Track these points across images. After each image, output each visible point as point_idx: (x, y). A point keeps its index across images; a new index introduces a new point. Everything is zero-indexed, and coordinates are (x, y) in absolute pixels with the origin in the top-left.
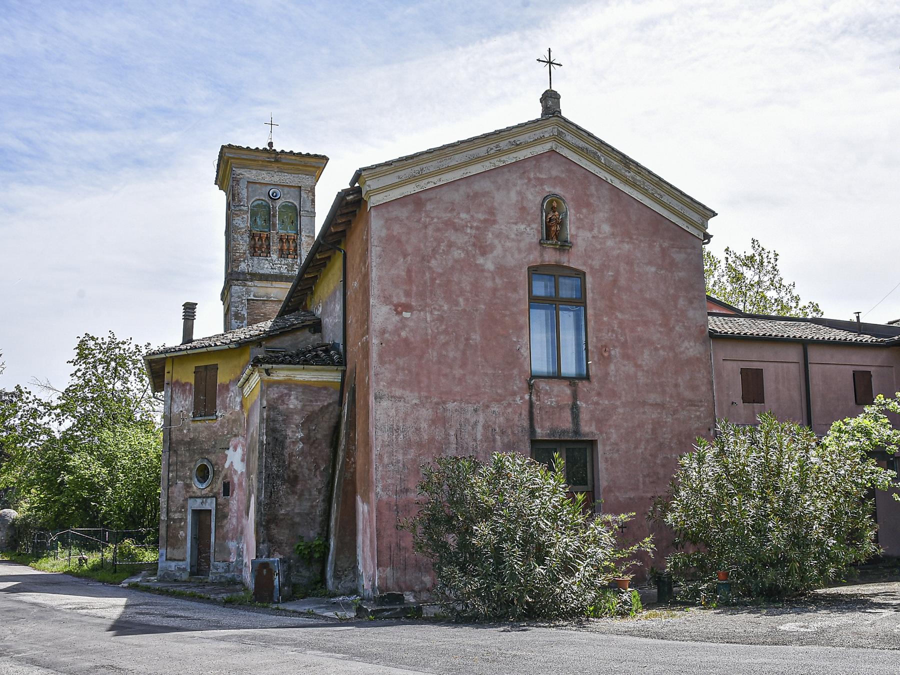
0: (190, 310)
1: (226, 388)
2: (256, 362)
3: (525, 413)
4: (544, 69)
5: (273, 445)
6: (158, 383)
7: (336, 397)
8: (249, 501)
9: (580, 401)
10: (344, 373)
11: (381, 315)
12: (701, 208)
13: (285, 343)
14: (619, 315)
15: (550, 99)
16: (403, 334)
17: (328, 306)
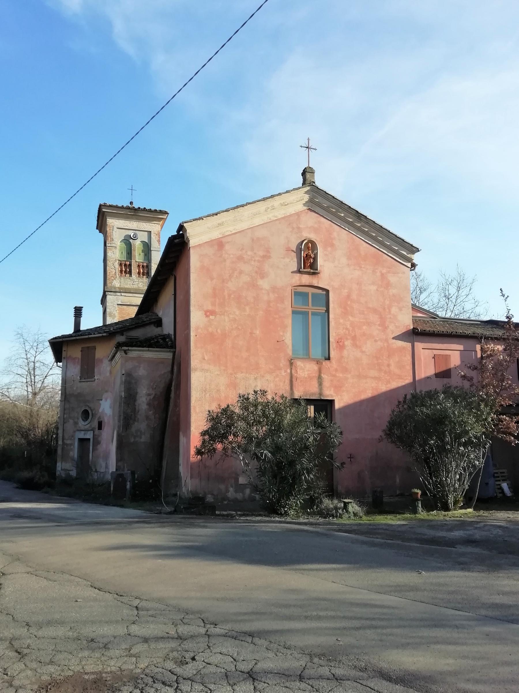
0: (78, 311)
1: (101, 361)
2: (119, 346)
3: (287, 382)
4: (305, 151)
5: (129, 397)
6: (58, 358)
7: (169, 369)
8: (113, 433)
9: (324, 374)
10: (174, 353)
11: (197, 318)
13: (139, 333)
14: (351, 318)
15: (307, 173)
16: (210, 330)
17: (164, 310)
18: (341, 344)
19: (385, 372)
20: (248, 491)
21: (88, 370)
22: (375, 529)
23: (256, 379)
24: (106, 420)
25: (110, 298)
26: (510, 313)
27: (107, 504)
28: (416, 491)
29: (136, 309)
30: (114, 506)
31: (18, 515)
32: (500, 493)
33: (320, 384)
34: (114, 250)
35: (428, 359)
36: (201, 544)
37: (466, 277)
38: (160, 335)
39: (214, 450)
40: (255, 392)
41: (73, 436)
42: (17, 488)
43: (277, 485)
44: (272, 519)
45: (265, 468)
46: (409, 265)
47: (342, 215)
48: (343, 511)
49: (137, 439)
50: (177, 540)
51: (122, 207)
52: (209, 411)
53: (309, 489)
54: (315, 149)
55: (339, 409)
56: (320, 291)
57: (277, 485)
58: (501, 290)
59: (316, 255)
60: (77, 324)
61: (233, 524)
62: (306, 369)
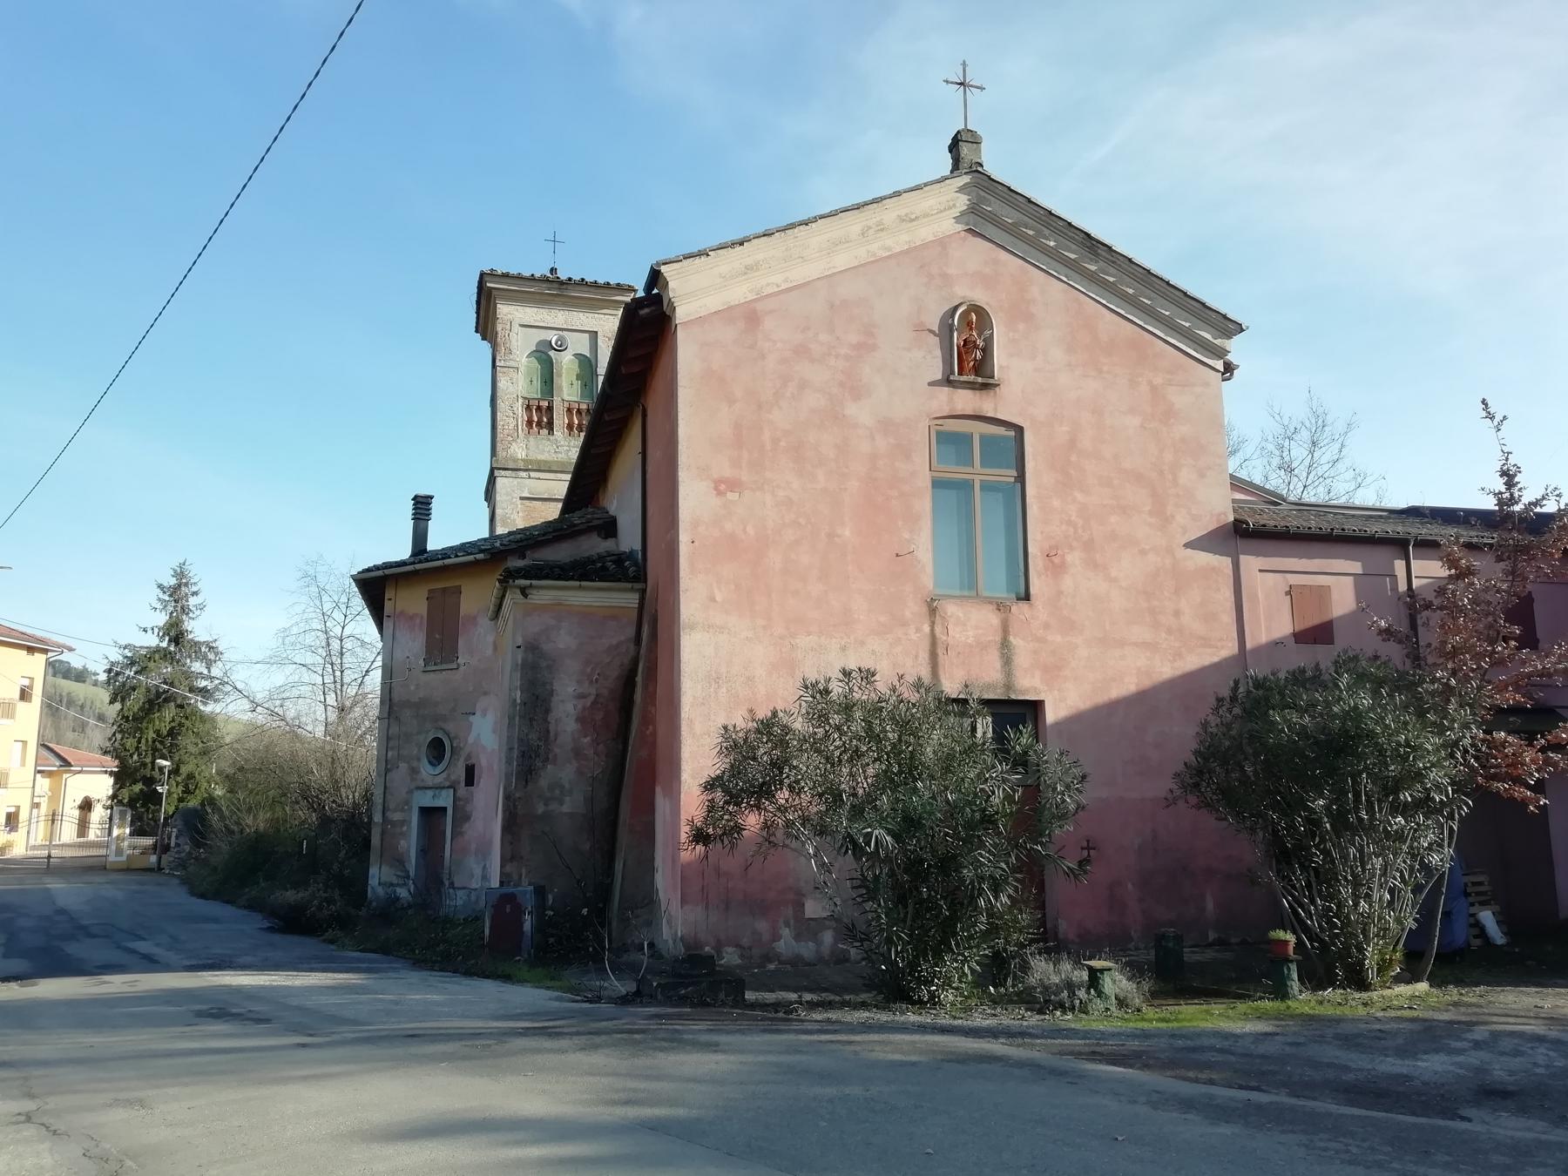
0: (422, 507)
1: (473, 620)
3: (924, 656)
4: (956, 93)
5: (534, 703)
12: (1220, 318)
13: (561, 553)
14: (1079, 496)
16: (728, 526)
17: (622, 500)
18: (1056, 560)
19: (1169, 631)
20: (828, 937)
21: (442, 643)
22: (1194, 1050)
23: (843, 649)
24: (483, 762)
25: (501, 483)
26: (1512, 461)
27: (469, 973)
28: (1281, 934)
29: (560, 505)
30: (487, 977)
31: (219, 1009)
32: (1475, 937)
33: (1007, 661)
34: (514, 375)
35: (1274, 600)
36: (694, 1113)
37: (1329, 420)
38: (609, 554)
39: (738, 829)
40: (846, 673)
41: (407, 803)
42: (271, 930)
43: (909, 922)
44: (899, 1018)
45: (876, 878)
46: (1219, 365)
47: (1052, 244)
48: (1088, 993)
49: (553, 806)
50: (623, 1096)
51: (532, 278)
52: (725, 728)
53: (993, 931)
54: (981, 88)
55: (1057, 724)
56: (1001, 431)
57: (909, 922)
58: (1484, 402)
59: (989, 341)
60: (420, 537)
61: (792, 1037)
62: (970, 624)
